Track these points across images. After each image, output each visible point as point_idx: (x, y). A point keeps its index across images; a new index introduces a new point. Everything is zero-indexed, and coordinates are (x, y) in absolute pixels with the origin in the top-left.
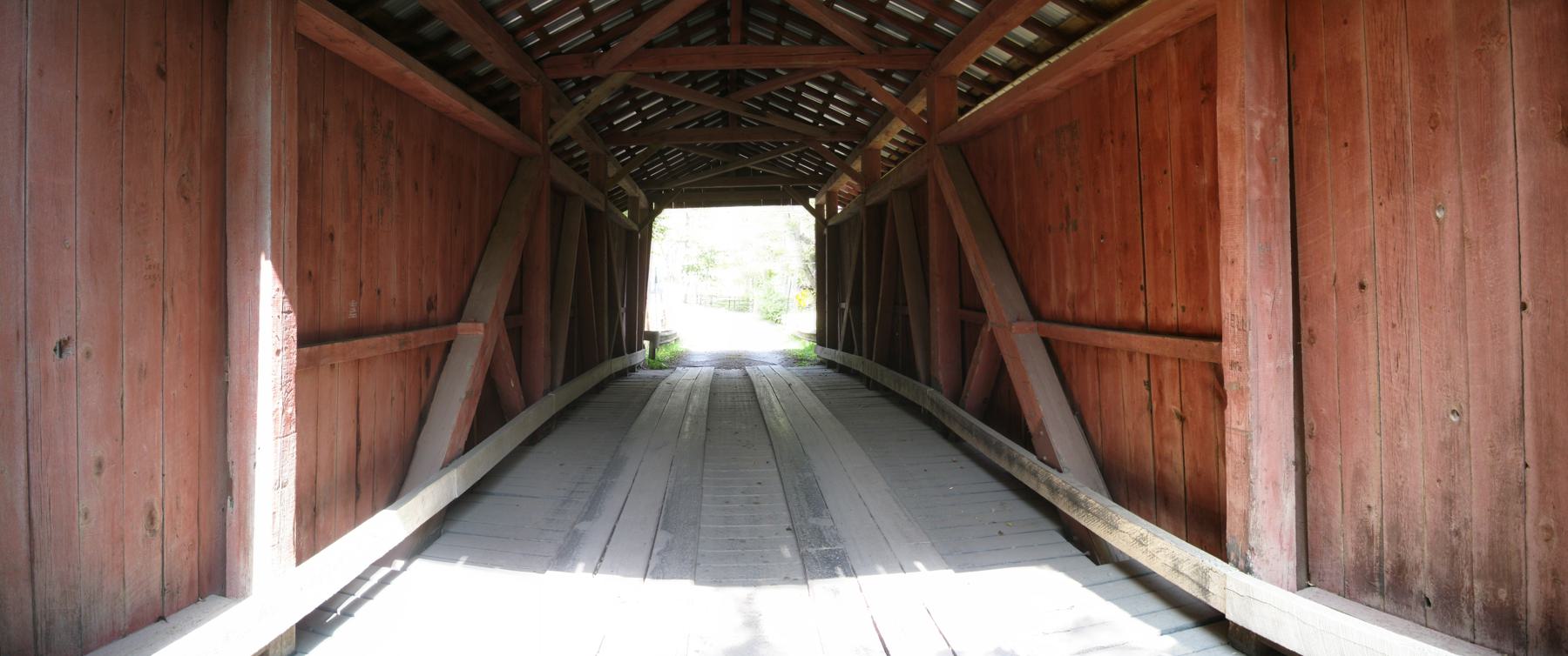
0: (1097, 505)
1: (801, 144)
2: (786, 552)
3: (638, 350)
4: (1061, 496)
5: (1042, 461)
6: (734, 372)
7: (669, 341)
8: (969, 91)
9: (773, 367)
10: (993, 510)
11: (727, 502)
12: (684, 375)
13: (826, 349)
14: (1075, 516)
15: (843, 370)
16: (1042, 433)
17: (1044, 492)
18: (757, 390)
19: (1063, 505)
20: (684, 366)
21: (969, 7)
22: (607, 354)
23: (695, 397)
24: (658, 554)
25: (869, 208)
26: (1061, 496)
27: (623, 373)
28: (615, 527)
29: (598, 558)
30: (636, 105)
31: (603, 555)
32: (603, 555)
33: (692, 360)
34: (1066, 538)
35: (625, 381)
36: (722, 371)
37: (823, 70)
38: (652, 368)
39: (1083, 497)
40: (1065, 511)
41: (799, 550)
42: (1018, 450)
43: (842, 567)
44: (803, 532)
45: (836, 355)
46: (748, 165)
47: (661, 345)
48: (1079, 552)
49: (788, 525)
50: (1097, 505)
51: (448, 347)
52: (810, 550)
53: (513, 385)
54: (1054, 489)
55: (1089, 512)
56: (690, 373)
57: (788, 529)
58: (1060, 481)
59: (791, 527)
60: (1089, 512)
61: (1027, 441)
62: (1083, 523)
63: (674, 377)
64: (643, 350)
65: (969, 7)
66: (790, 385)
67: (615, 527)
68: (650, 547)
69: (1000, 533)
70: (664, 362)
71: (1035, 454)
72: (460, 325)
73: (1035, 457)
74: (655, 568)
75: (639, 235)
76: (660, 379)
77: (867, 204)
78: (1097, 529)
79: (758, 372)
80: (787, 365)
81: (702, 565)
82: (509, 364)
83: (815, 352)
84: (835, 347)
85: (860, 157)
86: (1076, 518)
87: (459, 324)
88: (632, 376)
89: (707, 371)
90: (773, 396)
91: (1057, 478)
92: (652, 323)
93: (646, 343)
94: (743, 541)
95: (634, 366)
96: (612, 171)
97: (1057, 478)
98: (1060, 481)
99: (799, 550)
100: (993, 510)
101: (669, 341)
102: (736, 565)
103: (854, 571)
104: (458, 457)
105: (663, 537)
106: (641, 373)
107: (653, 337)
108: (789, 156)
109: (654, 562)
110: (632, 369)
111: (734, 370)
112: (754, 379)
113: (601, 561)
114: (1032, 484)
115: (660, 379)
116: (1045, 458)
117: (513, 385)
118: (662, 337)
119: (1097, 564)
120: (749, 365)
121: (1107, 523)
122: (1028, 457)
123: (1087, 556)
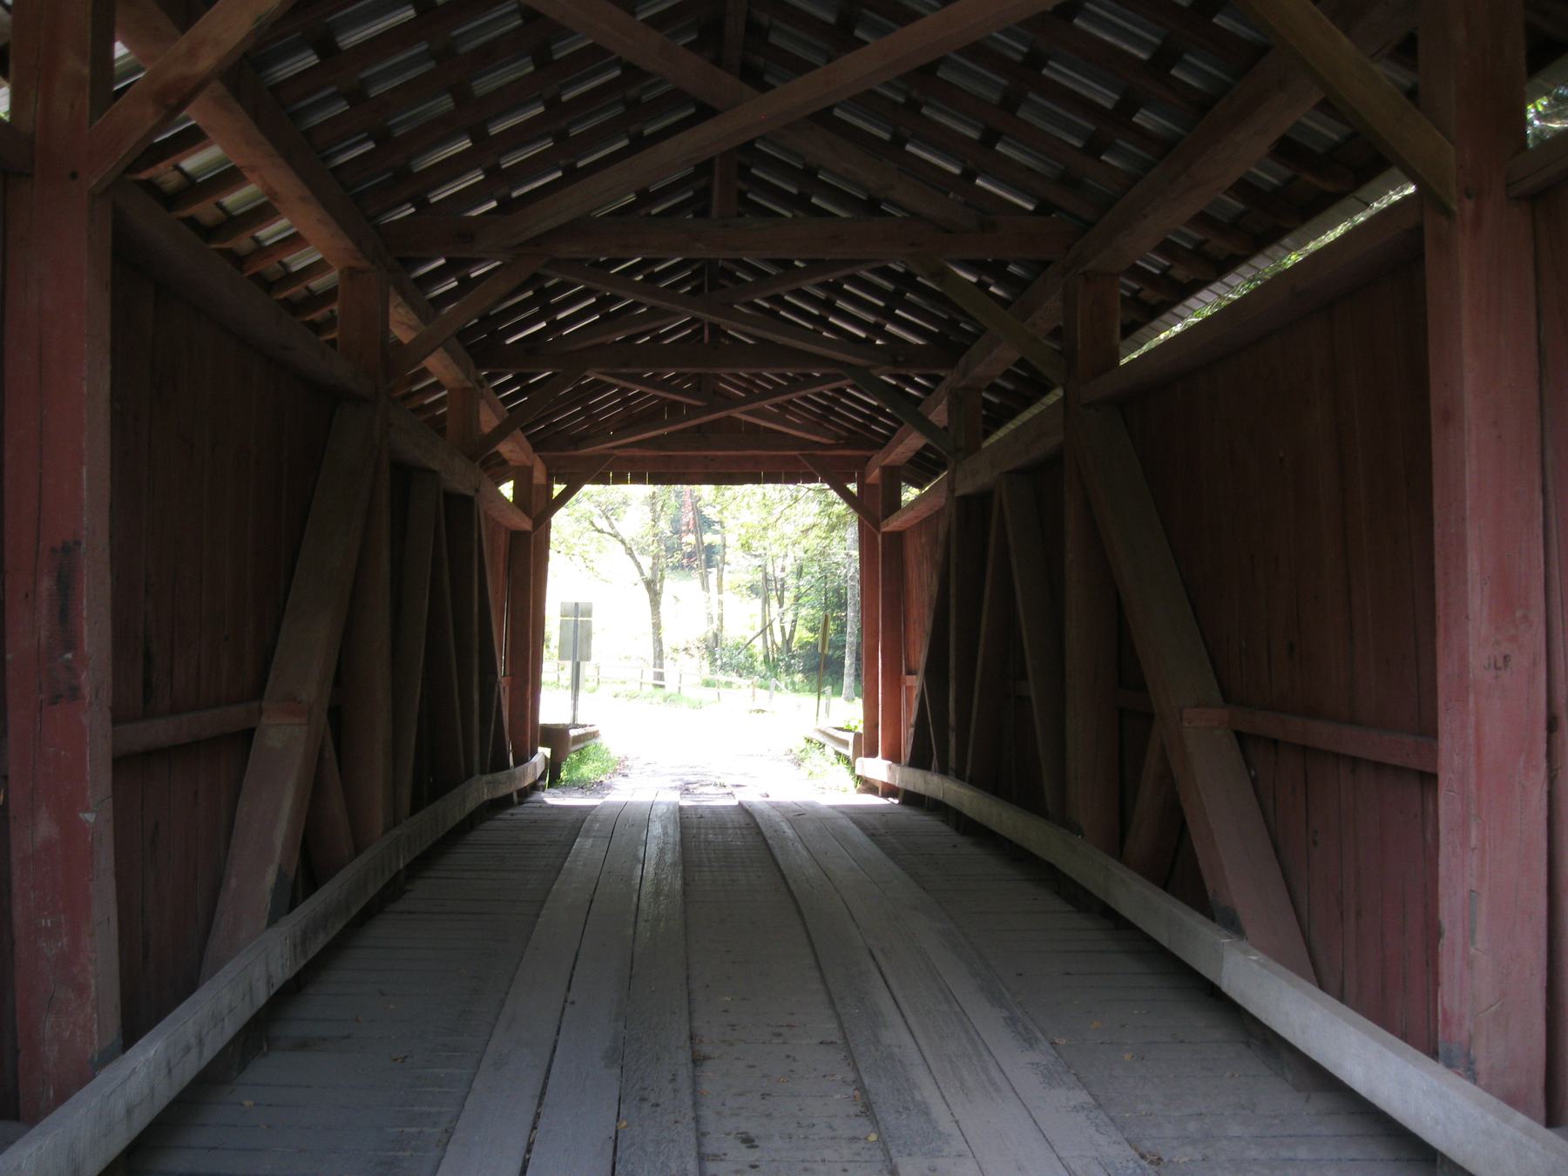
1: (825, 379)
8: (1165, 270)
21: (889, 423)
22: (477, 766)
25: (965, 499)
27: (504, 803)
30: (547, 312)
35: (520, 812)
37: (861, 262)
45: (918, 781)
46: (737, 413)
65: (889, 423)
77: (959, 493)
82: (330, 752)
85: (392, 289)
88: (532, 799)
96: (488, 420)
107: (555, 737)
108: (821, 395)
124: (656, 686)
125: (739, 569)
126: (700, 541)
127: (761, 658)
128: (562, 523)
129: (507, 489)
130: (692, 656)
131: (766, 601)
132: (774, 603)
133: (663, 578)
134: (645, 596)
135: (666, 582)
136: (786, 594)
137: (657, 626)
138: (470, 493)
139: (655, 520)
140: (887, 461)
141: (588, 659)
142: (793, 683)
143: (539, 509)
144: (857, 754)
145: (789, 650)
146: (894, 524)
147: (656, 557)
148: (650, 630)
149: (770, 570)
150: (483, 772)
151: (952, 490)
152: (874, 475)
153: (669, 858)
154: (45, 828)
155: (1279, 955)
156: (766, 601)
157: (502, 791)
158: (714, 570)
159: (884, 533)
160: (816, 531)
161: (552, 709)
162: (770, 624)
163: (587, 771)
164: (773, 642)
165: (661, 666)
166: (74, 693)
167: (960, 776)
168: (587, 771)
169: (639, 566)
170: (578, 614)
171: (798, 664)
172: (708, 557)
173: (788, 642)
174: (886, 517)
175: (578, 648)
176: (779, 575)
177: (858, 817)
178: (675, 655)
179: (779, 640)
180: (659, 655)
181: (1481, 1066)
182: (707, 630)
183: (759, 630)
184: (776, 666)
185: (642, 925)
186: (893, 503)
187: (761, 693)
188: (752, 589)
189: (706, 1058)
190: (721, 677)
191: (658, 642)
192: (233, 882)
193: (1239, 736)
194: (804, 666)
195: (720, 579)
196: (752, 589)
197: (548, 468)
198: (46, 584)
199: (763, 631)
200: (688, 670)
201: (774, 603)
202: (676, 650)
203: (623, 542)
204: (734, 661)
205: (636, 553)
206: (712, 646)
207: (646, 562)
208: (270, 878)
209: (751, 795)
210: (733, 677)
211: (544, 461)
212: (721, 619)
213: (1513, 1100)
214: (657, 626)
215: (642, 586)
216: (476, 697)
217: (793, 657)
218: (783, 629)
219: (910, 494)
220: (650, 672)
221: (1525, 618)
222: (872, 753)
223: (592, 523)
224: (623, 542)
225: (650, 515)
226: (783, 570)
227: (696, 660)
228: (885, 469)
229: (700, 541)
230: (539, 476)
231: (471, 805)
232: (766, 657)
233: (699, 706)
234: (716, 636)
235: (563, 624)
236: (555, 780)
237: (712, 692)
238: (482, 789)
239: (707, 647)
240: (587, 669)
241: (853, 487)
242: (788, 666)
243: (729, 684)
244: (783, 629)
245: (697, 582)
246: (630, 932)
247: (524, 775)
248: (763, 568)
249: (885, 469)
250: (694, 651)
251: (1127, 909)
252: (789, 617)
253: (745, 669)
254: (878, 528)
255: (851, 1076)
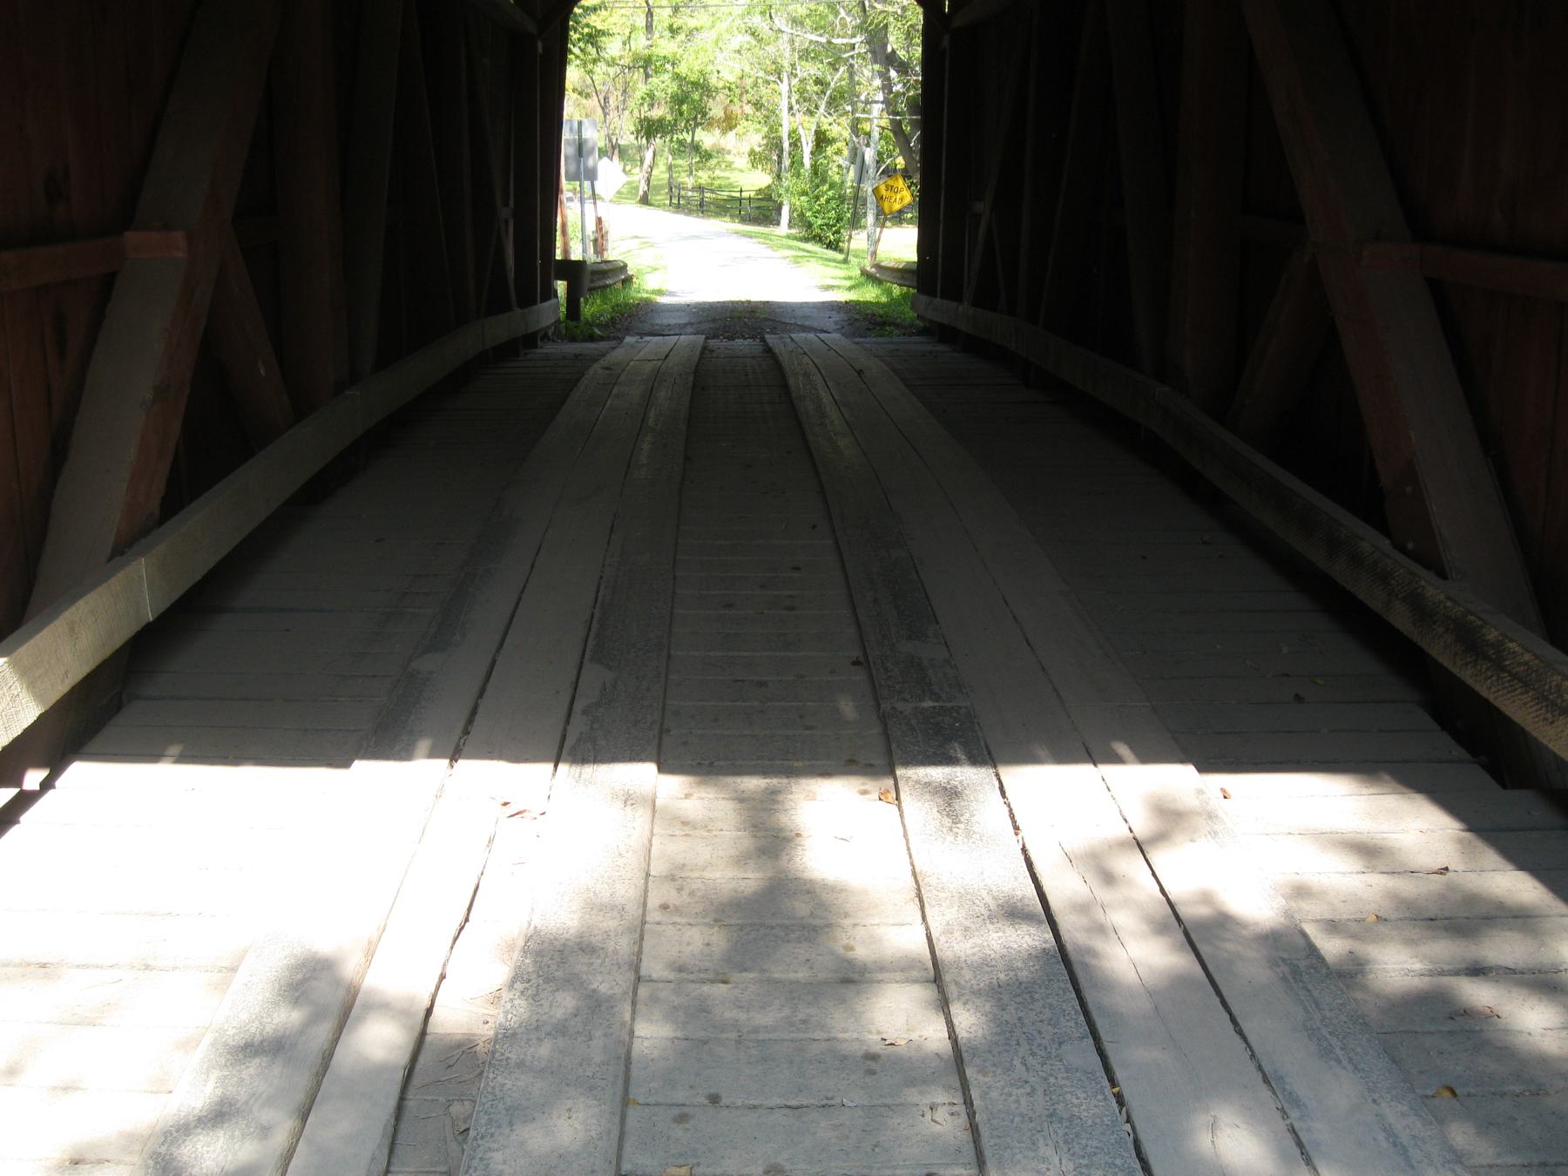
0: (1527, 657)
2: (848, 708)
3: (541, 302)
4: (1441, 630)
5: (1402, 549)
6: (743, 345)
7: (609, 282)
9: (822, 336)
10: (1285, 650)
11: (728, 606)
12: (639, 350)
13: (938, 301)
14: (1467, 675)
15: (972, 345)
16: (1409, 489)
17: (1401, 618)
18: (791, 381)
19: (1441, 650)
20: (642, 335)
23: (662, 395)
24: (585, 712)
26: (1441, 630)
28: (494, 662)
29: (460, 726)
31: (470, 721)
32: (470, 721)
33: (658, 321)
34: (1440, 724)
36: (713, 343)
38: (573, 339)
39: (1492, 635)
40: (1444, 660)
41: (878, 706)
42: (1350, 523)
43: (960, 743)
44: (886, 670)
45: (958, 313)
47: (591, 290)
48: (1467, 756)
49: (856, 653)
50: (1527, 657)
51: (106, 286)
52: (900, 706)
53: (263, 372)
54: (1423, 611)
55: (1503, 669)
56: (654, 345)
57: (856, 663)
58: (1442, 597)
59: (862, 660)
60: (1503, 669)
61: (1373, 509)
62: (1484, 693)
63: (618, 355)
64: (553, 301)
66: (860, 372)
67: (494, 662)
68: (568, 699)
69: (1298, 699)
70: (600, 326)
71: (1387, 533)
72: (131, 238)
73: (1387, 542)
74: (579, 740)
75: (540, 45)
76: (582, 363)
78: (1519, 709)
79: (791, 346)
80: (853, 335)
81: (673, 732)
83: (913, 308)
84: (958, 298)
86: (1470, 681)
87: (127, 234)
89: (688, 341)
90: (824, 394)
91: (1433, 590)
92: (573, 244)
93: (561, 286)
94: (762, 684)
95: (535, 334)
97: (1433, 590)
98: (1442, 597)
99: (878, 706)
100: (1285, 650)
101: (609, 282)
102: (746, 732)
103: (990, 753)
104: (145, 532)
105: (595, 676)
106: (549, 349)
107: (572, 270)
109: (579, 724)
110: (531, 340)
111: (739, 341)
112: (784, 359)
113: (466, 732)
114: (1373, 598)
115: (582, 363)
116: (1410, 546)
117: (263, 372)
118: (594, 273)
119: (1504, 786)
120: (774, 331)
121: (1547, 699)
122: (1371, 541)
123: (1483, 766)
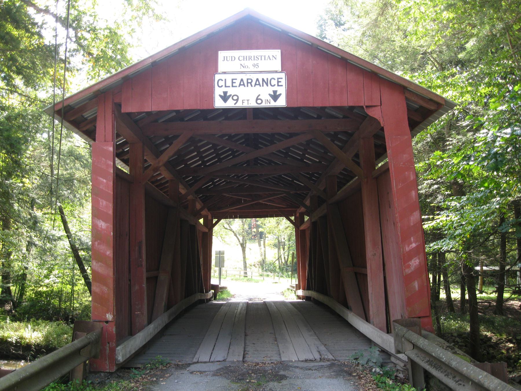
45: (310, 293)
77: (312, 221)
107: (215, 288)
124: (244, 276)
125: (270, 239)
126: (258, 231)
127: (278, 267)
128: (216, 229)
129: (201, 221)
130: (256, 267)
131: (279, 249)
132: (282, 250)
133: (246, 243)
134: (240, 248)
135: (247, 244)
136: (285, 247)
137: (244, 258)
138: (194, 224)
139: (243, 225)
140: (300, 211)
141: (224, 267)
142: (288, 275)
143: (210, 226)
144: (297, 289)
145: (287, 264)
146: (302, 227)
147: (243, 237)
148: (242, 259)
149: (280, 239)
150: (198, 292)
151: (311, 220)
152: (298, 215)
153: (243, 309)
154: (137, 287)
155: (359, 315)
156: (279, 249)
157: (203, 298)
158: (263, 240)
159: (300, 230)
160: (289, 228)
161: (214, 281)
162: (281, 256)
163: (225, 296)
164: (282, 262)
165: (246, 270)
166: (142, 265)
167: (315, 290)
168: (225, 296)
169: (238, 239)
170: (221, 254)
171: (290, 269)
172: (261, 236)
173: (286, 262)
174: (301, 225)
175: (221, 263)
176: (283, 240)
177: (293, 304)
178: (251, 267)
179: (283, 261)
180: (245, 267)
181: (375, 323)
182: (260, 259)
183: (277, 258)
184: (283, 270)
185: (236, 318)
186: (302, 221)
187: (276, 278)
188: (275, 245)
189: (247, 335)
190: (265, 273)
191: (245, 263)
192: (156, 305)
193: (356, 274)
194: (292, 269)
195: (264, 242)
196: (275, 245)
197: (212, 215)
198: (137, 248)
199: (278, 259)
200: (255, 272)
201: (282, 250)
202: (251, 265)
203: (233, 232)
204: (269, 269)
205: (238, 235)
206: (263, 264)
207: (241, 238)
208: (163, 304)
209: (268, 300)
210: (269, 273)
211: (211, 213)
212: (265, 256)
213: (383, 330)
214: (244, 258)
215: (240, 246)
216: (197, 274)
217: (288, 267)
218: (285, 258)
219: (306, 218)
220: (242, 273)
221: (378, 247)
222: (300, 289)
223: (224, 226)
224: (233, 232)
225: (242, 223)
226: (284, 239)
227: (257, 268)
228: (300, 213)
229: (258, 231)
230: (210, 217)
231: (196, 299)
232: (280, 267)
233: (257, 282)
234: (263, 261)
235: (216, 257)
236: (215, 299)
237: (262, 278)
238: (198, 296)
239: (261, 264)
240: (223, 269)
241: (293, 218)
242: (287, 270)
243: (268, 276)
244: (285, 258)
245: (257, 244)
246: (234, 319)
247: (208, 295)
248: (278, 238)
249: (300, 213)
250: (257, 266)
251: (338, 311)
252: (287, 254)
253: (273, 271)
254: (299, 229)
255: (274, 337)
